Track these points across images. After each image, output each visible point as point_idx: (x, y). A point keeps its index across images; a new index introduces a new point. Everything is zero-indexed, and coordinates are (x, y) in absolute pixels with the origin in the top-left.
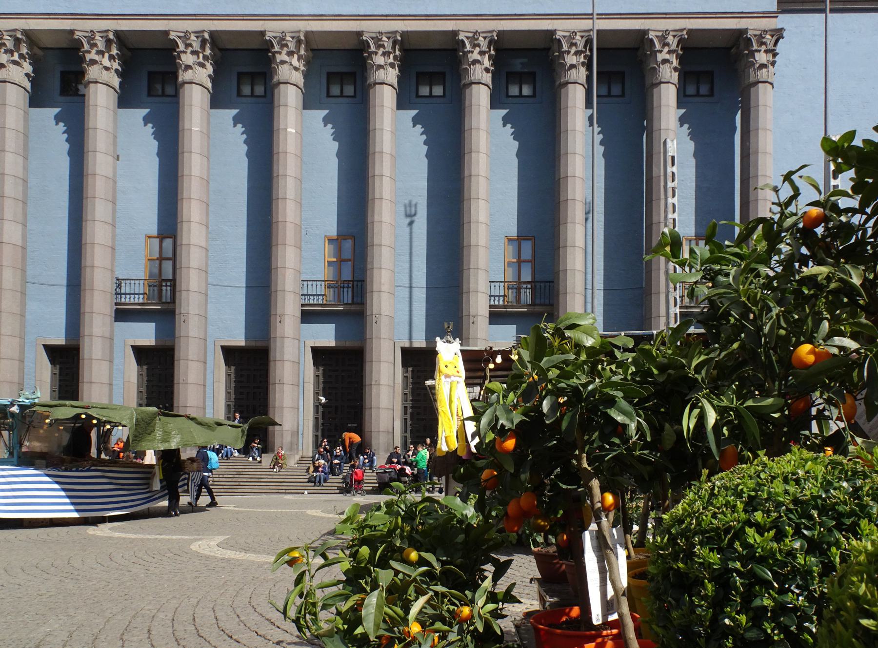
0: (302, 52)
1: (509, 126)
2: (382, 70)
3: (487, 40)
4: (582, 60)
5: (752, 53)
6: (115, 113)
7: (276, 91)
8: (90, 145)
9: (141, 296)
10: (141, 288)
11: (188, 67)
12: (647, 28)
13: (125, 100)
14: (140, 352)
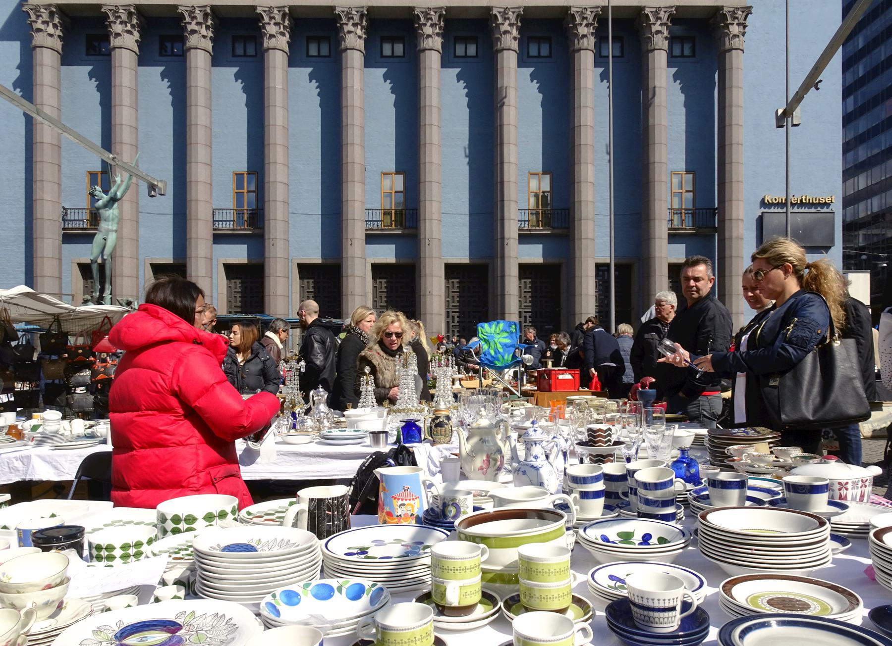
0: (364, 23)
1: (314, 81)
2: (430, 39)
3: (515, 14)
4: (591, 30)
5: (727, 26)
6: (59, 71)
7: (344, 55)
8: (116, 100)
9: (379, 223)
10: (230, 215)
11: (272, 36)
12: (643, 5)
13: (143, 60)
14: (231, 270)
